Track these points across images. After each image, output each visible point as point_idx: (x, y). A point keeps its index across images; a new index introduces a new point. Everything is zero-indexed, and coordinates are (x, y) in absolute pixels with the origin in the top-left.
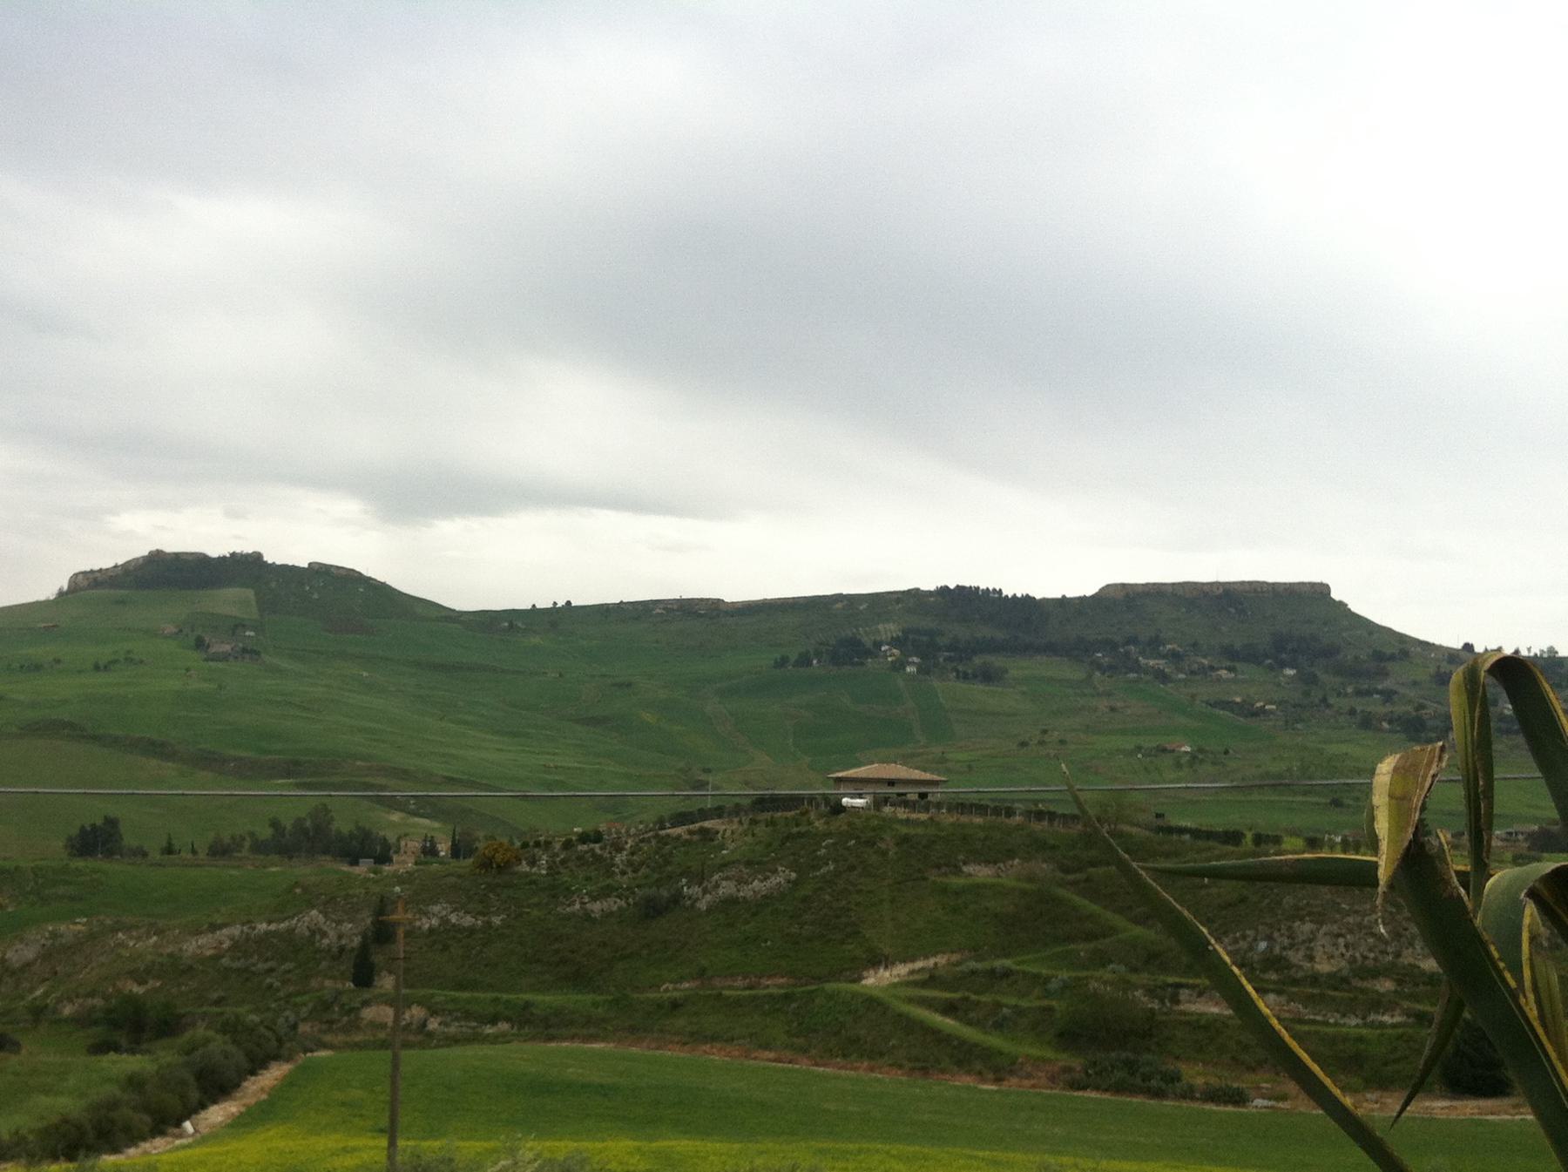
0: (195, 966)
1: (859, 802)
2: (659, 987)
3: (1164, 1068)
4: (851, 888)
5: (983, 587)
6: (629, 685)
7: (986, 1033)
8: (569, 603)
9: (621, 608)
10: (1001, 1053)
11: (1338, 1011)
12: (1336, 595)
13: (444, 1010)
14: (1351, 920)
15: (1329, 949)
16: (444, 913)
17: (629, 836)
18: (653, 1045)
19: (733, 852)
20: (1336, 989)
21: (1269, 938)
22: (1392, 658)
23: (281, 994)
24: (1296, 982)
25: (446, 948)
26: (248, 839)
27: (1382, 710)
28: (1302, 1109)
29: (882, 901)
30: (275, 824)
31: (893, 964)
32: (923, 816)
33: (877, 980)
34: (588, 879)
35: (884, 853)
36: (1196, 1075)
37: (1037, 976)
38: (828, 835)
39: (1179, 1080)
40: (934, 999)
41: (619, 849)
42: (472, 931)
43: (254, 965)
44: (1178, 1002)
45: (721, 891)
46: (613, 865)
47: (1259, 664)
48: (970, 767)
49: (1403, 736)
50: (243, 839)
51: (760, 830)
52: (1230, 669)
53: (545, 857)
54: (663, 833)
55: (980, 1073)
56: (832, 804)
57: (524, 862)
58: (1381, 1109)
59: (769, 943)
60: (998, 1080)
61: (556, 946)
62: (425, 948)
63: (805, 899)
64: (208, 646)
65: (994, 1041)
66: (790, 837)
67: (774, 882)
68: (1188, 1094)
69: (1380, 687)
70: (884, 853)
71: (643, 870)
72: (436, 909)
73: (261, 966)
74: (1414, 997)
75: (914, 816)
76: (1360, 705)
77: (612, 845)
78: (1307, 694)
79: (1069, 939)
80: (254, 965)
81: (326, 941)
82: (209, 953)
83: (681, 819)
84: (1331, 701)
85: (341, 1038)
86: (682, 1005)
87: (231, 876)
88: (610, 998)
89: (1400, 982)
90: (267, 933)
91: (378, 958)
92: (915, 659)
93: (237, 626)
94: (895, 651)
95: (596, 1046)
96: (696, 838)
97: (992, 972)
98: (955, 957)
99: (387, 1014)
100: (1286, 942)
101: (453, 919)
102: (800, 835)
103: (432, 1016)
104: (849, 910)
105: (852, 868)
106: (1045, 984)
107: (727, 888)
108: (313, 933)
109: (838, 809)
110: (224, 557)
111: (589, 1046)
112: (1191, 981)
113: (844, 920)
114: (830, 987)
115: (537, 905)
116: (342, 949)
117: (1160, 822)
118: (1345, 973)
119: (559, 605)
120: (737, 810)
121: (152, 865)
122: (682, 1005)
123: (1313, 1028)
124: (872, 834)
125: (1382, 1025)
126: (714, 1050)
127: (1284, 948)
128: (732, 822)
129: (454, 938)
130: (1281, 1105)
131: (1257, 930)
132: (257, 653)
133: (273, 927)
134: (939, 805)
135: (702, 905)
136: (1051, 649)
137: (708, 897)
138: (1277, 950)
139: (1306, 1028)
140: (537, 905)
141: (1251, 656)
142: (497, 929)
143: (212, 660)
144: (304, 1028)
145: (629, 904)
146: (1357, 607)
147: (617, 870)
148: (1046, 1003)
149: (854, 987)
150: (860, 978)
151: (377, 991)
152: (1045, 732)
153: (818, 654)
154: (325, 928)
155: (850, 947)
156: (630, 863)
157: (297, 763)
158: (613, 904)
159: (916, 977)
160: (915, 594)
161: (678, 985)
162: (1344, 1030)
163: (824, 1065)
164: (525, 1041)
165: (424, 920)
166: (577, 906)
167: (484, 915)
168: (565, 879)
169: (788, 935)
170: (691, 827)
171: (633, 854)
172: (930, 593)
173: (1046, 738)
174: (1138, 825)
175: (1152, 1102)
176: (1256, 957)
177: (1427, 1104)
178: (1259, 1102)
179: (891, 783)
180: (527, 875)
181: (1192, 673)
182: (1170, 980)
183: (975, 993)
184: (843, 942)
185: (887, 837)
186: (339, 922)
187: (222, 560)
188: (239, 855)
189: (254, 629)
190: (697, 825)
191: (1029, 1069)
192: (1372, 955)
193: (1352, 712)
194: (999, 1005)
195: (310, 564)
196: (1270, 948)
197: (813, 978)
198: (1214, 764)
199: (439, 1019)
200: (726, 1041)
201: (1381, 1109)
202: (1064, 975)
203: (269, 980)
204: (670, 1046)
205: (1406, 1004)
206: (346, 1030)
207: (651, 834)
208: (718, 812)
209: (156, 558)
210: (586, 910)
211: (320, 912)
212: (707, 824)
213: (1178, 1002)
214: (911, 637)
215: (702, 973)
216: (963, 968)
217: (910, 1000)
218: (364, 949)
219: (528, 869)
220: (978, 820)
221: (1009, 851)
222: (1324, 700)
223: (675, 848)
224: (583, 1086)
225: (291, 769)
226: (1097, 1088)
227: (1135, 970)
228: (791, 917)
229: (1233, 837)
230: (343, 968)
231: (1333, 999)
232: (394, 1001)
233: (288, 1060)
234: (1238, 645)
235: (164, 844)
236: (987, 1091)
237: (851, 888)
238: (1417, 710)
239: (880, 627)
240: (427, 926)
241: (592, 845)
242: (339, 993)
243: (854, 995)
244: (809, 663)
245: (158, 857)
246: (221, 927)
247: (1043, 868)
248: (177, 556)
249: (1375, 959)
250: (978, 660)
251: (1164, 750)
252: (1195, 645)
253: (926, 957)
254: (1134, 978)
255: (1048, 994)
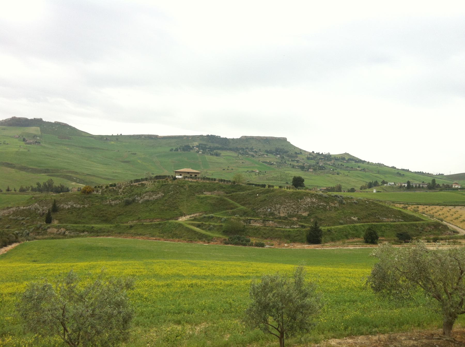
0: (2, 218)
1: (180, 177)
2: (128, 222)
3: (246, 239)
4: (177, 197)
5: (216, 135)
6: (135, 154)
7: (206, 231)
8: (121, 134)
9: (134, 136)
10: (210, 236)
11: (285, 225)
12: (288, 140)
13: (70, 229)
14: (288, 204)
15: (283, 211)
16: (72, 204)
17: (123, 185)
18: (125, 237)
19: (149, 189)
20: (285, 220)
21: (271, 208)
22: (298, 154)
23: (26, 226)
24: (276, 218)
25: (72, 213)
26: (31, 188)
27: (296, 164)
28: (277, 248)
29: (184, 201)
30: (38, 184)
31: (186, 215)
32: (195, 181)
33: (182, 220)
34: (112, 196)
35: (185, 189)
36: (253, 240)
37: (219, 218)
38: (171, 185)
39: (250, 241)
40: (195, 224)
41: (120, 188)
42: (79, 209)
43: (19, 218)
44: (250, 223)
45: (145, 198)
46: (118, 192)
47: (273, 154)
48: (212, 174)
49: (300, 170)
50: (29, 187)
51: (156, 183)
52: (267, 155)
53: (100, 190)
54: (132, 184)
55: (204, 241)
56: (174, 177)
57: (95, 191)
58: (293, 247)
59: (156, 211)
60: (208, 243)
61: (102, 212)
62: (66, 213)
63: (166, 200)
64: (26, 141)
65: (208, 233)
66: (163, 185)
67: (158, 196)
68: (251, 245)
69: (296, 160)
70: (185, 189)
71: (126, 193)
72: (70, 203)
73: (21, 218)
74: (300, 222)
75: (193, 180)
76: (292, 163)
77: (119, 187)
78: (282, 160)
79: (227, 209)
80: (19, 218)
81: (39, 212)
82: (7, 215)
83: (137, 181)
84: (286, 162)
85: (41, 237)
86: (133, 227)
87: (25, 197)
88: (115, 225)
89: (298, 218)
90: (23, 210)
91: (53, 216)
92: (201, 150)
93: (35, 136)
94: (197, 149)
95: (110, 237)
96: (140, 185)
97: (209, 217)
98: (201, 214)
99: (55, 230)
100: (274, 209)
101: (74, 205)
102: (165, 185)
103: (67, 231)
104: (176, 203)
105: (178, 193)
106: (221, 220)
107: (147, 198)
108: (36, 209)
109: (175, 178)
110: (32, 119)
111: (108, 237)
112: (253, 218)
113: (175, 205)
114: (170, 221)
115: (97, 202)
116: (43, 214)
117: (248, 183)
118: (286, 216)
119: (119, 135)
120: (151, 179)
121: (2, 194)
122: (133, 227)
123: (279, 229)
124: (183, 185)
125: (294, 228)
126: (140, 238)
127: (274, 211)
128: (149, 182)
129: (74, 211)
130: (272, 247)
131: (268, 206)
132: (40, 143)
133: (25, 208)
134: (199, 178)
135: (140, 202)
136: (231, 149)
137: (142, 200)
138: (272, 211)
139: (278, 229)
140: (97, 202)
141: (271, 152)
142: (86, 208)
143: (27, 144)
144: (31, 234)
145: (122, 202)
146: (292, 143)
147: (119, 193)
148: (221, 224)
149: (176, 221)
150: (178, 219)
151: (52, 224)
152: (228, 167)
153: (180, 148)
154: (39, 208)
155: (176, 212)
156: (123, 192)
157: (48, 170)
158: (117, 202)
159: (192, 219)
160: (202, 136)
161: (133, 222)
162: (286, 229)
163: (167, 240)
164: (91, 237)
165: (66, 206)
166: (108, 202)
167: (83, 204)
168: (105, 195)
169: (161, 209)
170: (139, 183)
171: (124, 189)
172: (205, 136)
173: (229, 168)
174: (244, 184)
175: (243, 247)
176: (268, 213)
177: (304, 246)
178: (267, 246)
179: (188, 173)
180: (95, 195)
181: (259, 155)
182: (249, 218)
183: (205, 222)
184: (174, 210)
185: (186, 185)
186: (43, 207)
187: (31, 120)
188: (28, 192)
189: (39, 137)
190: (141, 183)
191: (216, 240)
192: (292, 212)
193: (291, 164)
194: (210, 225)
195: (55, 122)
196: (271, 211)
197: (167, 219)
198: (263, 174)
199: (68, 231)
200: (143, 235)
201: (293, 247)
202: (225, 217)
203: (22, 222)
204: (129, 237)
205: (299, 223)
206: (42, 235)
207: (129, 185)
208: (146, 179)
209: (14, 119)
210: (110, 203)
211: (38, 204)
212: (143, 182)
213: (250, 223)
214: (201, 146)
215: (139, 219)
216: (203, 216)
217: (189, 224)
218: (49, 213)
219: (96, 193)
220: (208, 182)
221: (214, 189)
222: (285, 162)
223: (135, 188)
224: (101, 248)
225: (46, 171)
226: (231, 244)
227: (241, 216)
228: (162, 204)
229: (264, 186)
230: (43, 219)
231: (284, 222)
232: (58, 227)
233: (19, 242)
234: (268, 150)
235: (7, 189)
236: (205, 245)
237: (177, 197)
238: (303, 164)
239: (194, 143)
240: (67, 207)
241: (113, 187)
242: (41, 225)
243: (176, 223)
244: (178, 150)
245: (5, 192)
246: (10, 208)
247: (222, 193)
248: (19, 118)
249: (293, 213)
250: (215, 151)
251: (253, 171)
252: (260, 150)
253: (194, 214)
254: (241, 218)
255: (222, 222)
